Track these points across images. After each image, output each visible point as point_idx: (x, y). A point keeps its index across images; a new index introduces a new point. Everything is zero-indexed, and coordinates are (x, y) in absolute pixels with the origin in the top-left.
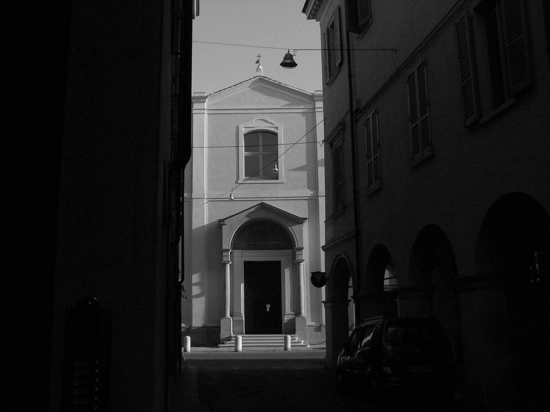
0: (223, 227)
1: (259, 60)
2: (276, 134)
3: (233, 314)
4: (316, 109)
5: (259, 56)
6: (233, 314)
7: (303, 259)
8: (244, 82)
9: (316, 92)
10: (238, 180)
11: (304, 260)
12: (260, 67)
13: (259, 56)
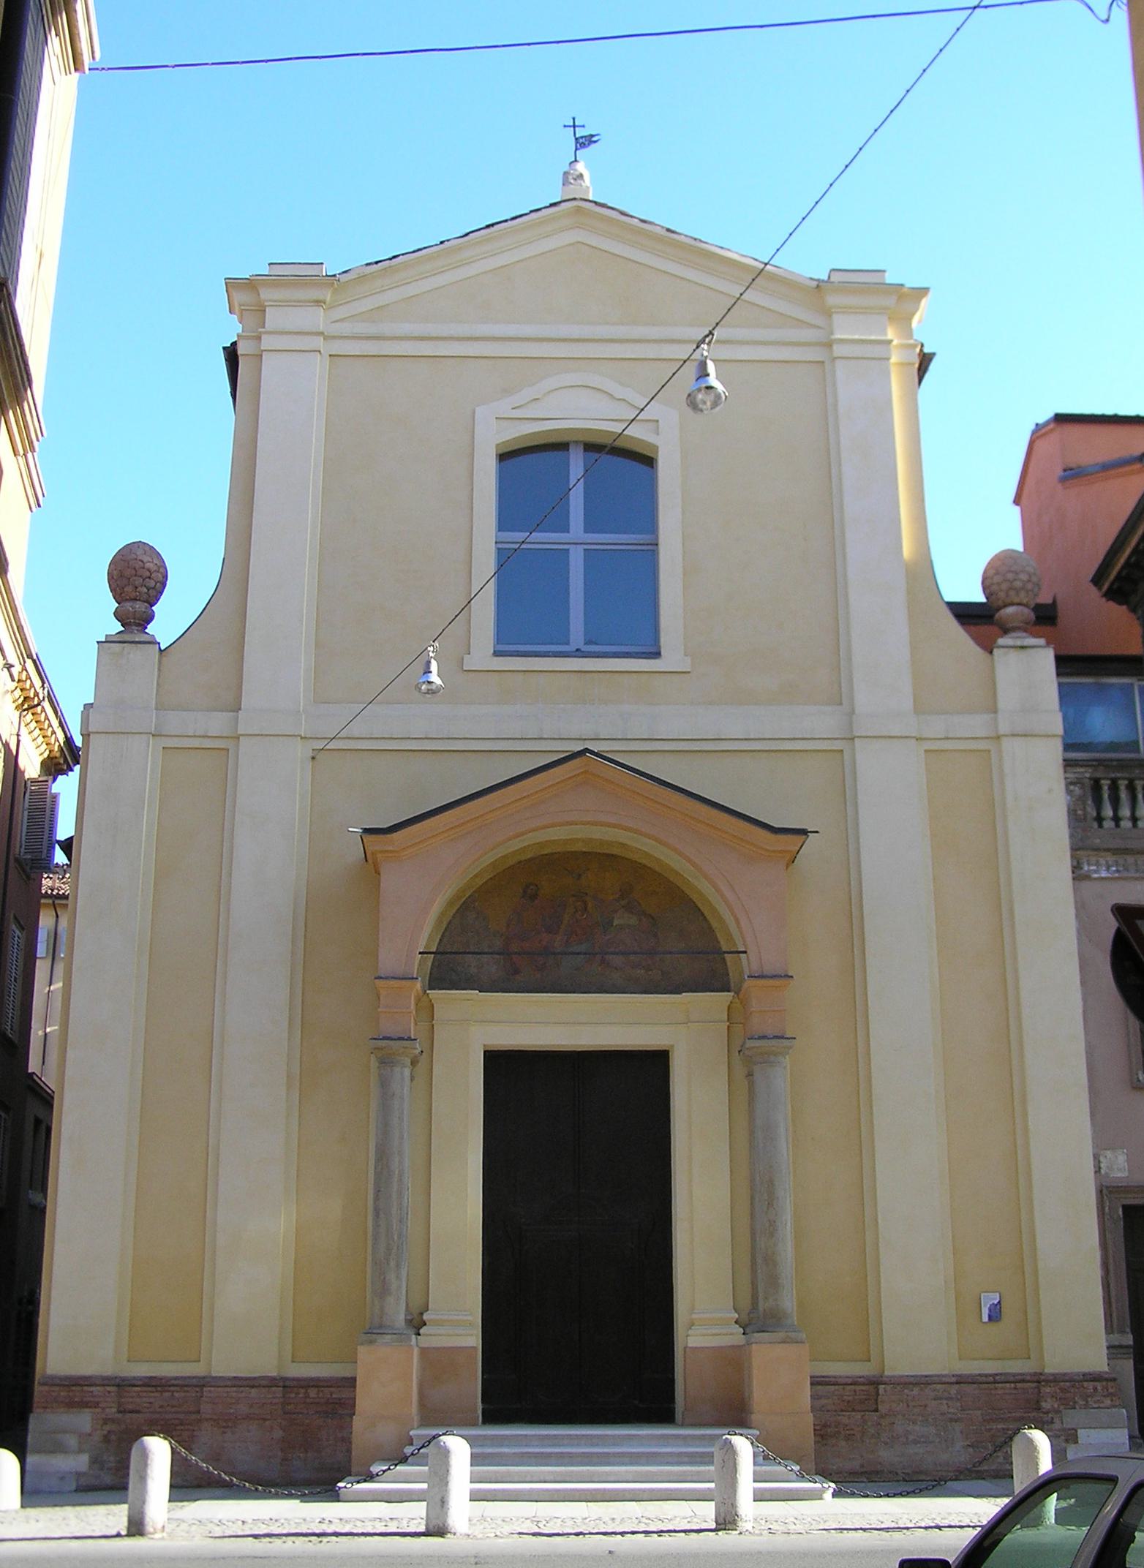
0: (37, 964)
1: (576, 149)
2: (647, 461)
3: (425, 1317)
4: (835, 347)
5: (574, 126)
6: (425, 1317)
7: (790, 974)
8: (506, 221)
9: (833, 273)
10: (466, 657)
11: (792, 977)
12: (580, 167)
13: (574, 126)
